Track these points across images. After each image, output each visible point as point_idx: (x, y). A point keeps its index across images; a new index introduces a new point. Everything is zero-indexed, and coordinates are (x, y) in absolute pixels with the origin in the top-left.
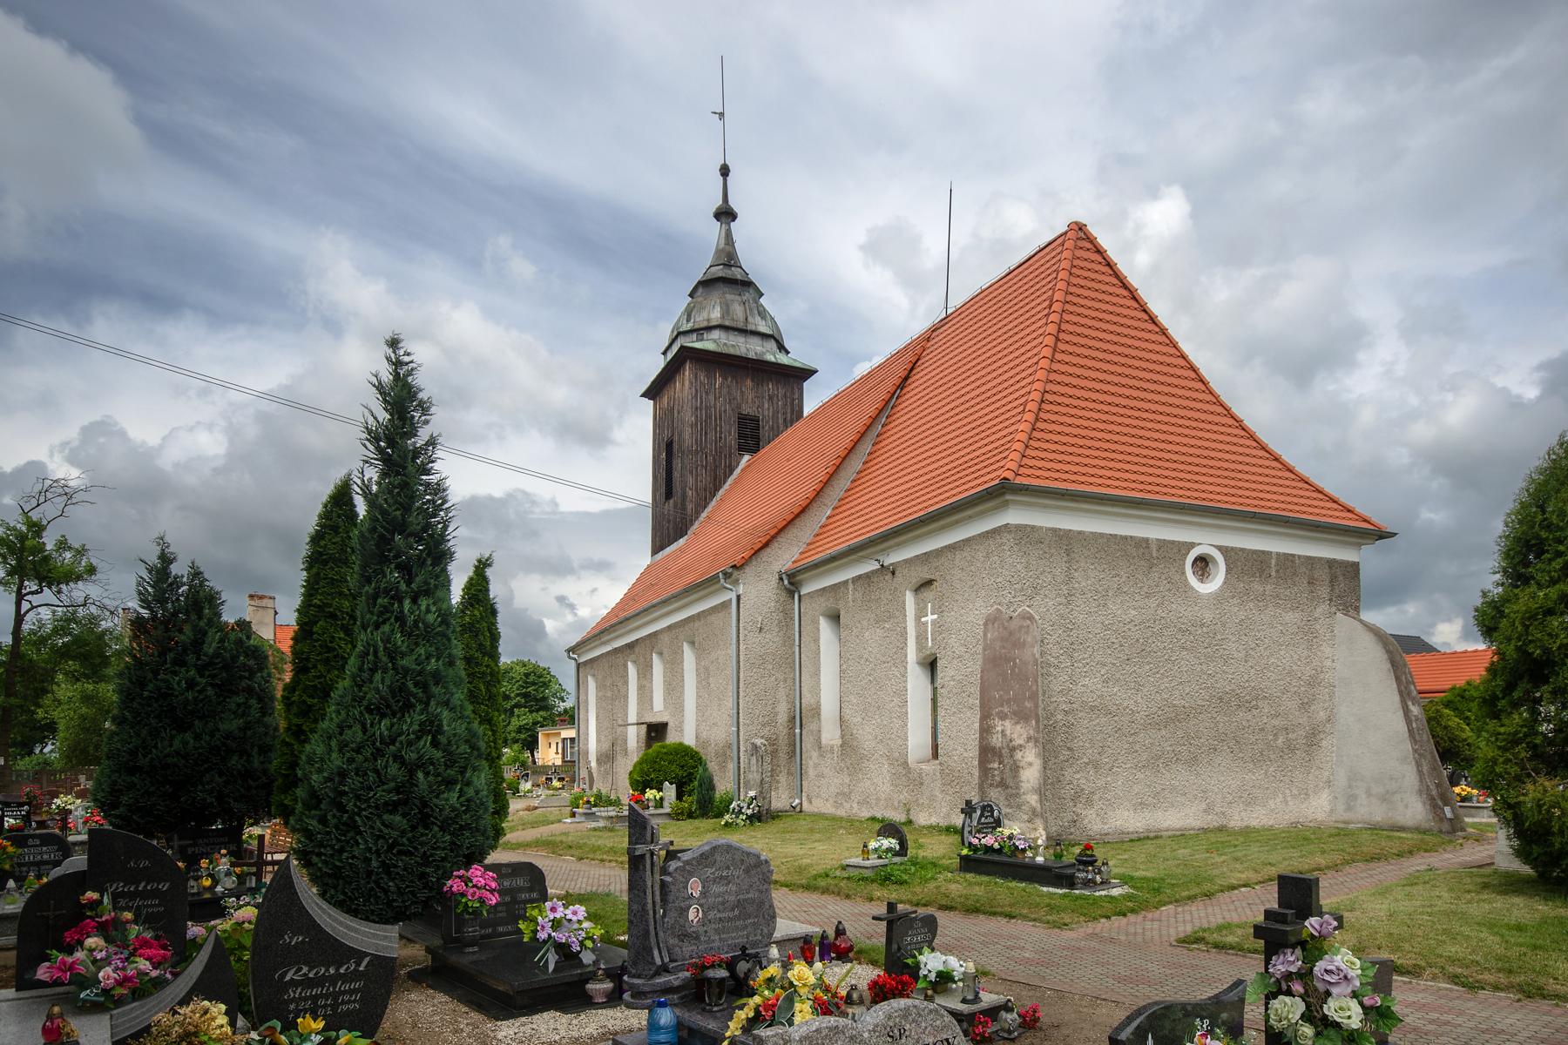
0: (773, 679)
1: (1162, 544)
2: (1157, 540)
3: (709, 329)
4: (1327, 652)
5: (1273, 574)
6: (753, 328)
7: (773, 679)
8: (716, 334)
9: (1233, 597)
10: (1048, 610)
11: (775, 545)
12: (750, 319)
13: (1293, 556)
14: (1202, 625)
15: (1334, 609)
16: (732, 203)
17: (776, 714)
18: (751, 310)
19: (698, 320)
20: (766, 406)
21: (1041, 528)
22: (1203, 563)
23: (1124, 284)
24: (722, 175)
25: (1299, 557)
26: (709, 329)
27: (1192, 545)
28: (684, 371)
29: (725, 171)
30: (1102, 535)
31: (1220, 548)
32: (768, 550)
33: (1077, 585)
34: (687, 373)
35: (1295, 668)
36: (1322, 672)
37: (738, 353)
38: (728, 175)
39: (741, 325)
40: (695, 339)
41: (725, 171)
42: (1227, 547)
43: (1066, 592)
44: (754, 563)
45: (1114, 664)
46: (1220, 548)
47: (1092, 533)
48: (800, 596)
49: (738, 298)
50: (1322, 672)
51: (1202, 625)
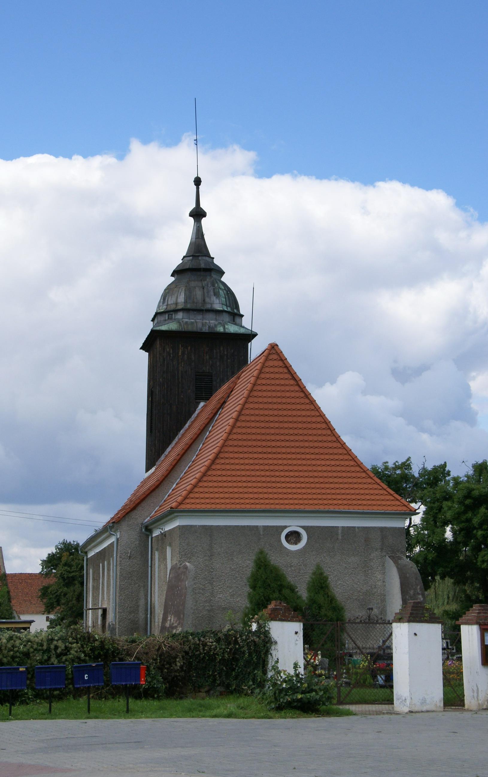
0: (137, 586)
1: (266, 528)
2: (263, 526)
3: (176, 311)
4: (379, 577)
5: (340, 537)
6: (208, 306)
7: (137, 586)
8: (180, 315)
9: (312, 551)
10: (200, 563)
11: (139, 508)
12: (207, 300)
13: (354, 527)
14: (291, 566)
15: (384, 554)
16: (202, 206)
17: (138, 606)
18: (208, 292)
19: (169, 303)
20: (218, 363)
21: (196, 526)
22: (294, 537)
23: (293, 377)
24: (195, 185)
25: (358, 527)
26: (176, 311)
27: (286, 527)
28: (157, 342)
29: (198, 182)
30: (230, 526)
31: (303, 527)
32: (136, 511)
33: (216, 551)
34: (158, 342)
35: (355, 586)
36: (375, 588)
37: (195, 329)
38: (200, 185)
39: (199, 306)
40: (167, 318)
41: (198, 182)
42: (308, 527)
43: (209, 554)
44: (127, 519)
45: (237, 587)
46: (303, 527)
47: (225, 526)
48: (152, 538)
49: (200, 284)
50: (375, 588)
51: (291, 566)
